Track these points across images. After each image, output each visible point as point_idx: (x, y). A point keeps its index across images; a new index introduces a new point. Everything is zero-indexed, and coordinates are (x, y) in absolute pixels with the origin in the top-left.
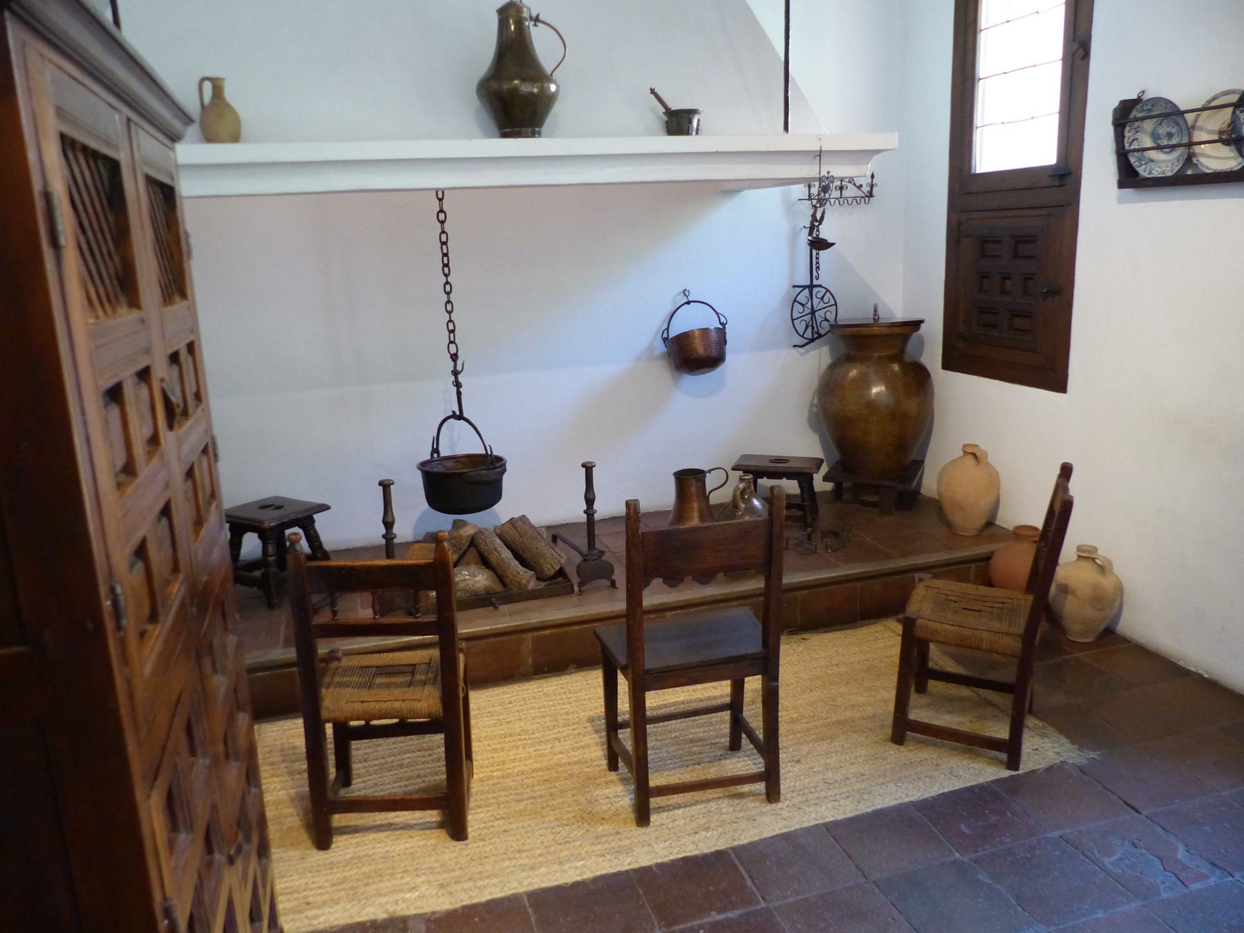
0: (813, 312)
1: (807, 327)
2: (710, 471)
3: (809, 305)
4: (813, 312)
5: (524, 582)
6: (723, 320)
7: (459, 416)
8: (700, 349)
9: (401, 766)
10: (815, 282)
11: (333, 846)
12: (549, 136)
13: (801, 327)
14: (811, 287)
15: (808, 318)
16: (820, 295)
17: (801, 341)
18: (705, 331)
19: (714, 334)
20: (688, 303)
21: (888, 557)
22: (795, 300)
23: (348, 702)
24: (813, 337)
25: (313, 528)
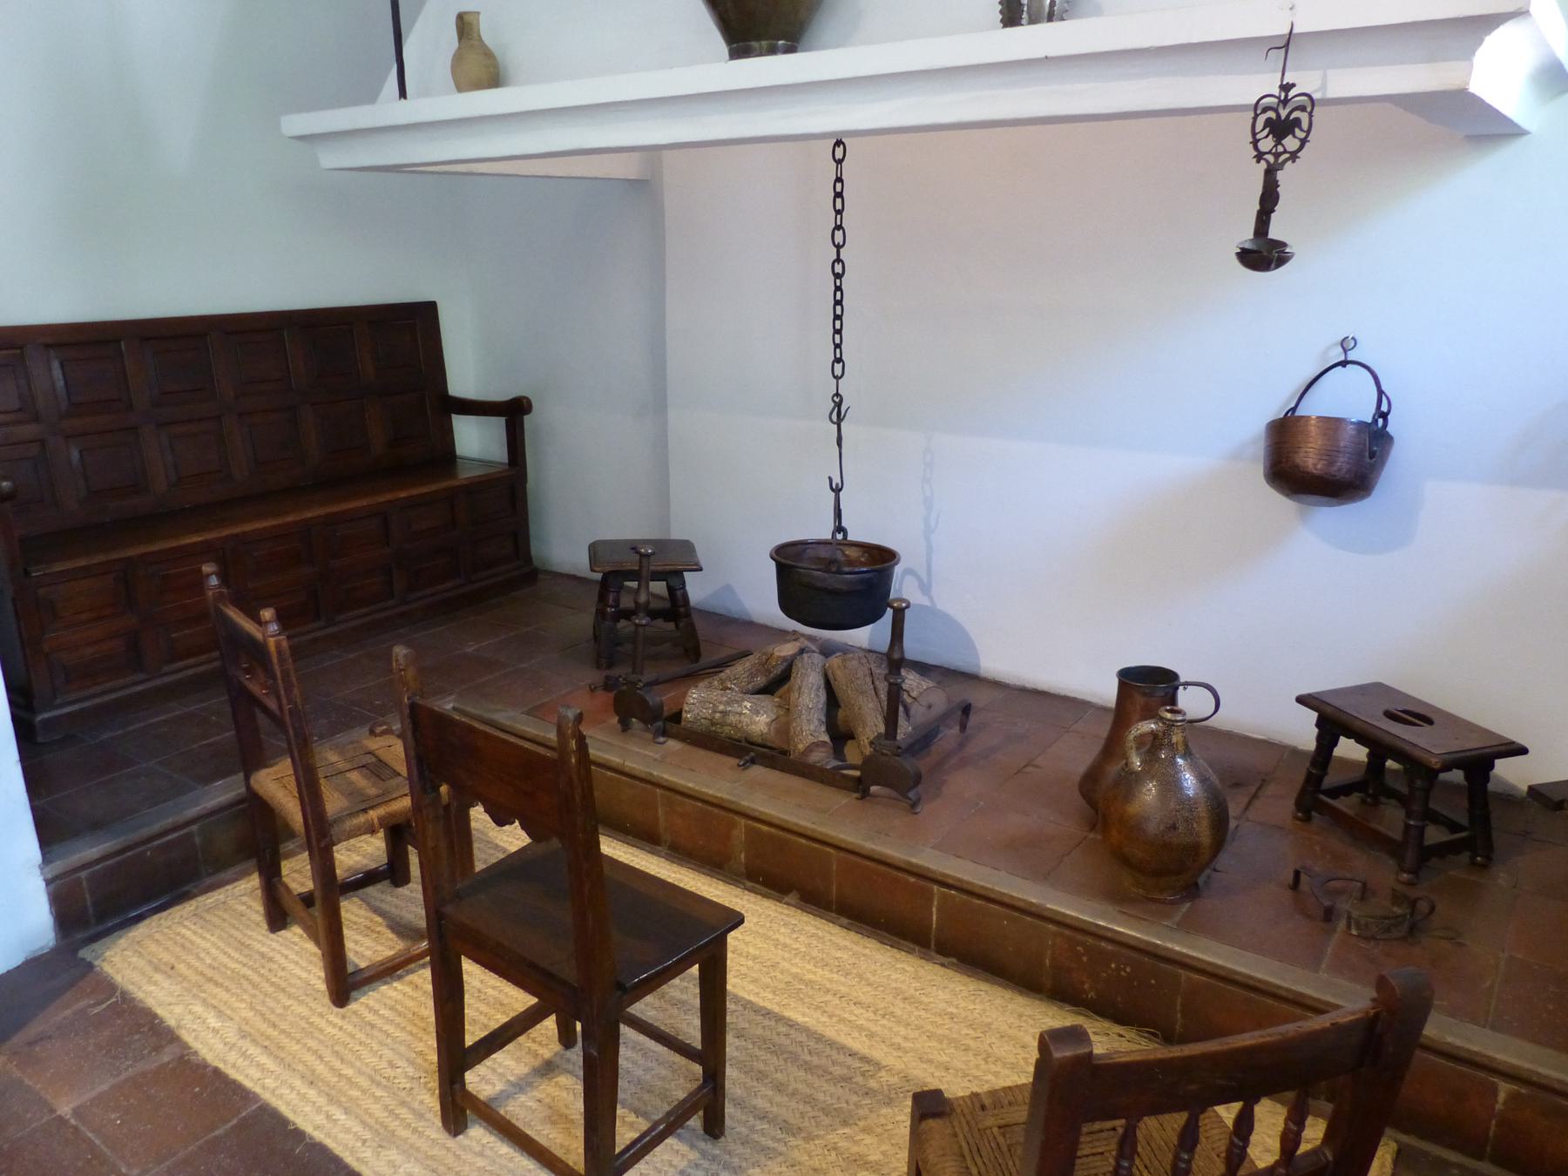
8: (1310, 458)
11: (282, 932)
20: (1344, 364)
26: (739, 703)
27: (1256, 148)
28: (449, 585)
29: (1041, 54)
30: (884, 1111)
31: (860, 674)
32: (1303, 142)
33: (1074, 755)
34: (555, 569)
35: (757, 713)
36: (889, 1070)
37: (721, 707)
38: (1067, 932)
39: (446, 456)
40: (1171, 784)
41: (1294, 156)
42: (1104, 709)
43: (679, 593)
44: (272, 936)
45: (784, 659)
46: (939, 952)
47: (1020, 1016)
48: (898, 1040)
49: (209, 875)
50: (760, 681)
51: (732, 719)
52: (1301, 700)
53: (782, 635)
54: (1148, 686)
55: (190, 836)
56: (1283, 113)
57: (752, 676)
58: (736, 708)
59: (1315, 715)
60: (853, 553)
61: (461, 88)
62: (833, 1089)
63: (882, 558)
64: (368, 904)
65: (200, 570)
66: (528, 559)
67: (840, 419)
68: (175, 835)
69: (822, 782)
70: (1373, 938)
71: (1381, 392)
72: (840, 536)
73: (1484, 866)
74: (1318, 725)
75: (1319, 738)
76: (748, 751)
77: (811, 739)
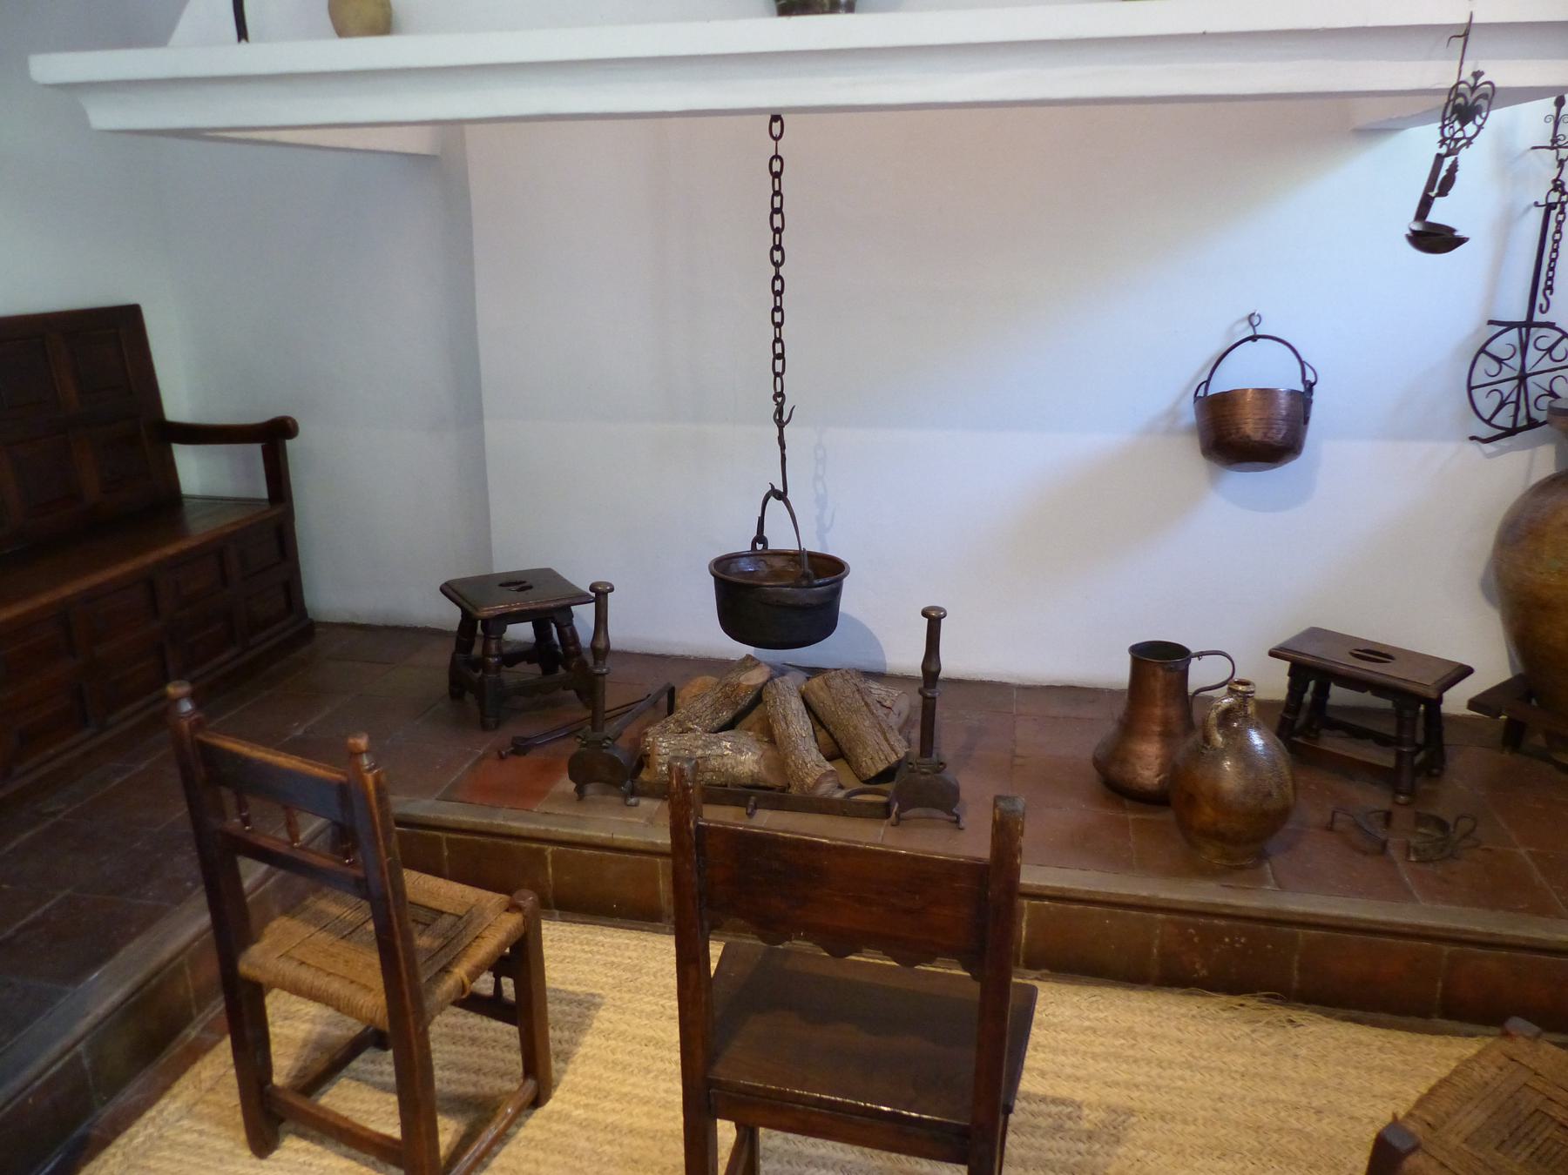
0: (1522, 378)
1: (1502, 404)
2: (1200, 655)
3: (1516, 362)
4: (1522, 378)
5: (809, 780)
6: (1310, 377)
7: (781, 496)
8: (1251, 427)
9: (473, 1041)
10: (1538, 317)
11: (276, 1154)
12: (862, 12)
13: (1487, 404)
14: (1529, 324)
15: (1506, 388)
16: (1544, 344)
17: (1485, 431)
18: (1267, 395)
19: (1283, 402)
20: (1254, 338)
21: (1542, 909)
22: (1483, 350)
23: (286, 956)
24: (1513, 423)
25: (570, 624)
26: (717, 744)
27: (1442, 133)
28: (225, 657)
29: (1200, 30)
30: (1121, 1151)
31: (848, 692)
32: (1480, 127)
33: (1082, 744)
34: (324, 619)
35: (741, 752)
36: (1089, 1105)
37: (699, 753)
38: (1176, 917)
39: (167, 499)
40: (1243, 752)
41: (1469, 142)
42: (1111, 693)
43: (567, 630)
44: (264, 1163)
45: (754, 686)
46: (1028, 967)
47: (1150, 1011)
48: (1069, 1070)
49: (104, 1104)
50: (726, 715)
51: (714, 763)
52: (1272, 654)
53: (748, 663)
54: (1159, 662)
55: (78, 1057)
56: (1471, 99)
57: (717, 711)
58: (715, 750)
59: (1288, 664)
60: (778, 563)
61: (342, 31)
62: (1053, 1143)
63: (831, 569)
64: (366, 1082)
65: (165, 697)
66: (303, 611)
67: (781, 425)
68: (60, 1065)
69: (845, 814)
70: (1431, 861)
71: (1302, 363)
72: (759, 547)
73: (1438, 776)
74: (1291, 674)
75: (1291, 686)
76: (748, 796)
77: (818, 772)
